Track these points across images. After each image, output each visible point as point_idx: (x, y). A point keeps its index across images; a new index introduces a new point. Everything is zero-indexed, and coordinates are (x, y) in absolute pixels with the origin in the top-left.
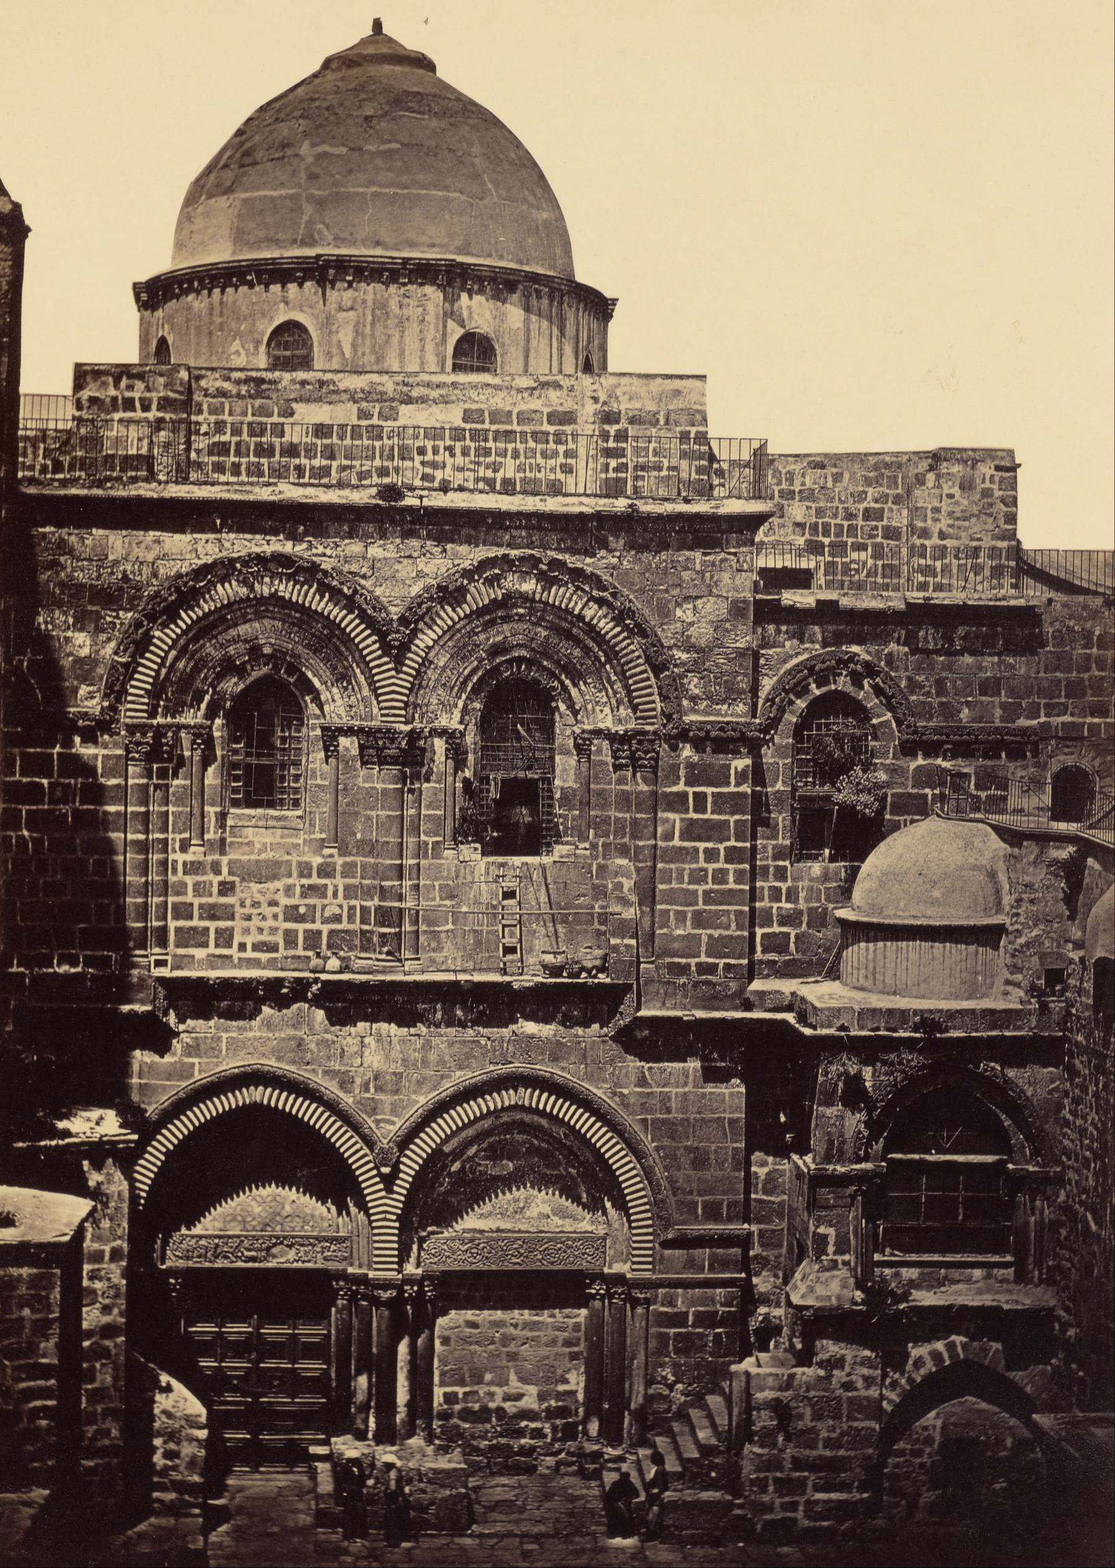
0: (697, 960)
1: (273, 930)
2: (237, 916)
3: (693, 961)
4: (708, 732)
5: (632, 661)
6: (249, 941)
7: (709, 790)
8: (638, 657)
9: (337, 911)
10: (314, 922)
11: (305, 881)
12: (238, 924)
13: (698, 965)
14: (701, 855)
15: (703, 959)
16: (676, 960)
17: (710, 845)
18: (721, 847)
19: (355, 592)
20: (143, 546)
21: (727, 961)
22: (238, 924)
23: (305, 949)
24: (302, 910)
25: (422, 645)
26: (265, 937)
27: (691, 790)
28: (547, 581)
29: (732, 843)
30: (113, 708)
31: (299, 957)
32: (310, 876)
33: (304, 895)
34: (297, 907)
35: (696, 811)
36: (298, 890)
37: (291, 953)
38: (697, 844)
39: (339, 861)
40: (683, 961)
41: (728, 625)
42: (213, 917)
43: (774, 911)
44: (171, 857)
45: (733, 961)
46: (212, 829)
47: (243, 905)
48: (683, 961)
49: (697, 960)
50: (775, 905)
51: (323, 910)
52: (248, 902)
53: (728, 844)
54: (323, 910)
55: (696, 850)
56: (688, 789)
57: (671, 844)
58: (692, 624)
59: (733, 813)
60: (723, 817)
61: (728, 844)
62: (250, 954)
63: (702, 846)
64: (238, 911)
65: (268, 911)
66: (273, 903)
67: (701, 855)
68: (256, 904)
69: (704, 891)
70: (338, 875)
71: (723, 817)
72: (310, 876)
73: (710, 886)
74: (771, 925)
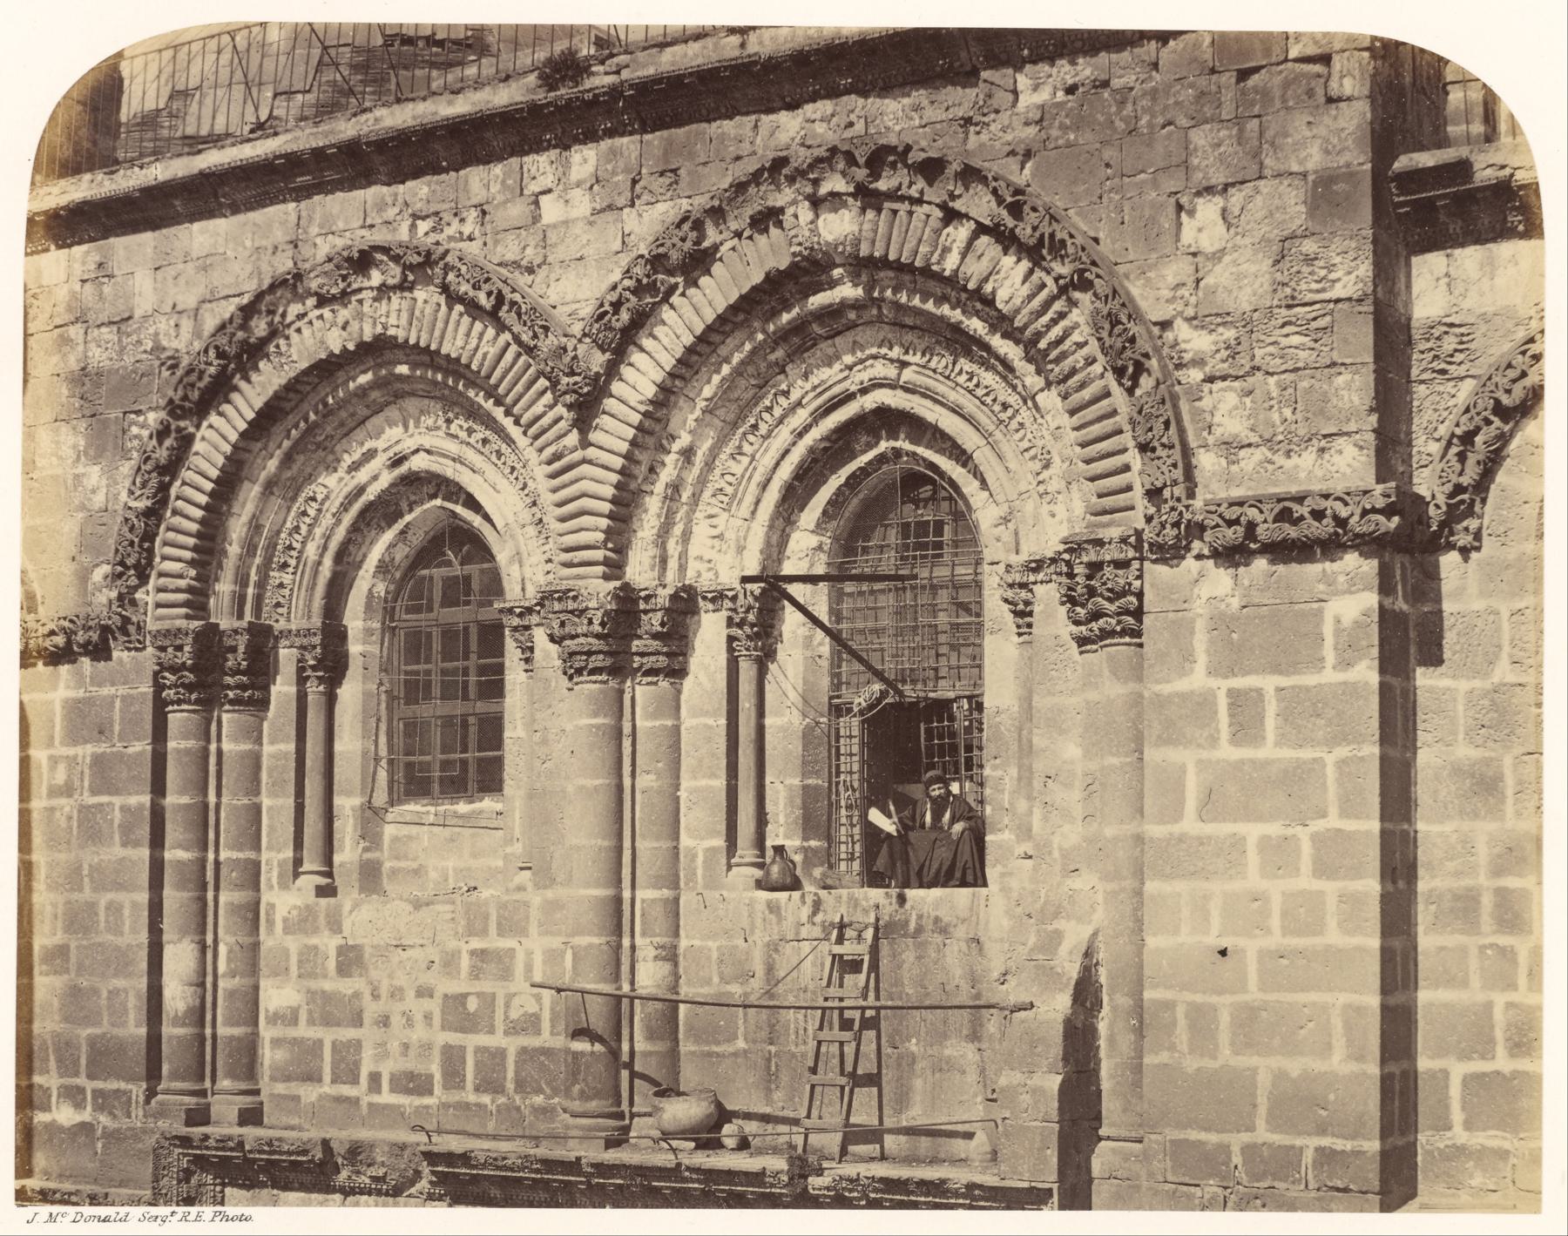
0: (1246, 1137)
1: (427, 1047)
2: (367, 1018)
3: (1237, 1141)
4: (1251, 527)
5: (1073, 372)
6: (386, 1070)
7: (1269, 683)
8: (1090, 361)
9: (532, 1007)
10: (491, 1031)
11: (476, 944)
12: (367, 1034)
13: (1249, 1150)
14: (1253, 858)
15: (1263, 1134)
16: (1194, 1135)
17: (1274, 829)
18: (1303, 835)
19: (500, 299)
20: (182, 280)
21: (1326, 1142)
22: (367, 1034)
23: (477, 1089)
24: (472, 1004)
25: (633, 397)
26: (410, 1064)
27: (1222, 686)
28: (618, 72)
29: (1333, 821)
30: (126, 599)
31: (467, 1106)
32: (484, 932)
33: (476, 974)
34: (463, 997)
35: (1235, 740)
36: (465, 962)
37: (455, 1097)
38: (1241, 828)
39: (536, 899)
40: (1213, 1138)
41: (1309, 246)
42: (328, 1021)
43: (1499, 1015)
44: (266, 897)
45: (1340, 1144)
46: (348, 842)
47: (376, 996)
48: (1213, 1138)
49: (1246, 1137)
50: (1500, 999)
51: (507, 1006)
52: (384, 991)
53: (1318, 825)
54: (507, 1006)
55: (1238, 843)
56: (1213, 683)
57: (1176, 829)
58: (1218, 256)
59: (1332, 742)
60: (1307, 754)
61: (1318, 825)
62: (386, 1097)
63: (1254, 832)
64: (371, 1009)
65: (418, 1007)
66: (424, 992)
67: (1253, 858)
68: (396, 993)
69: (1263, 954)
70: (533, 929)
71: (1307, 754)
72: (484, 932)
73: (1276, 940)
74: (1487, 1054)
